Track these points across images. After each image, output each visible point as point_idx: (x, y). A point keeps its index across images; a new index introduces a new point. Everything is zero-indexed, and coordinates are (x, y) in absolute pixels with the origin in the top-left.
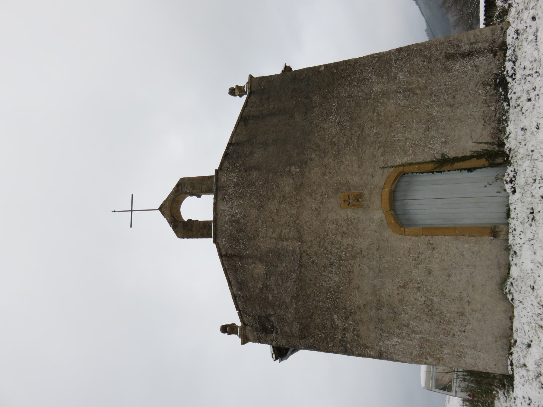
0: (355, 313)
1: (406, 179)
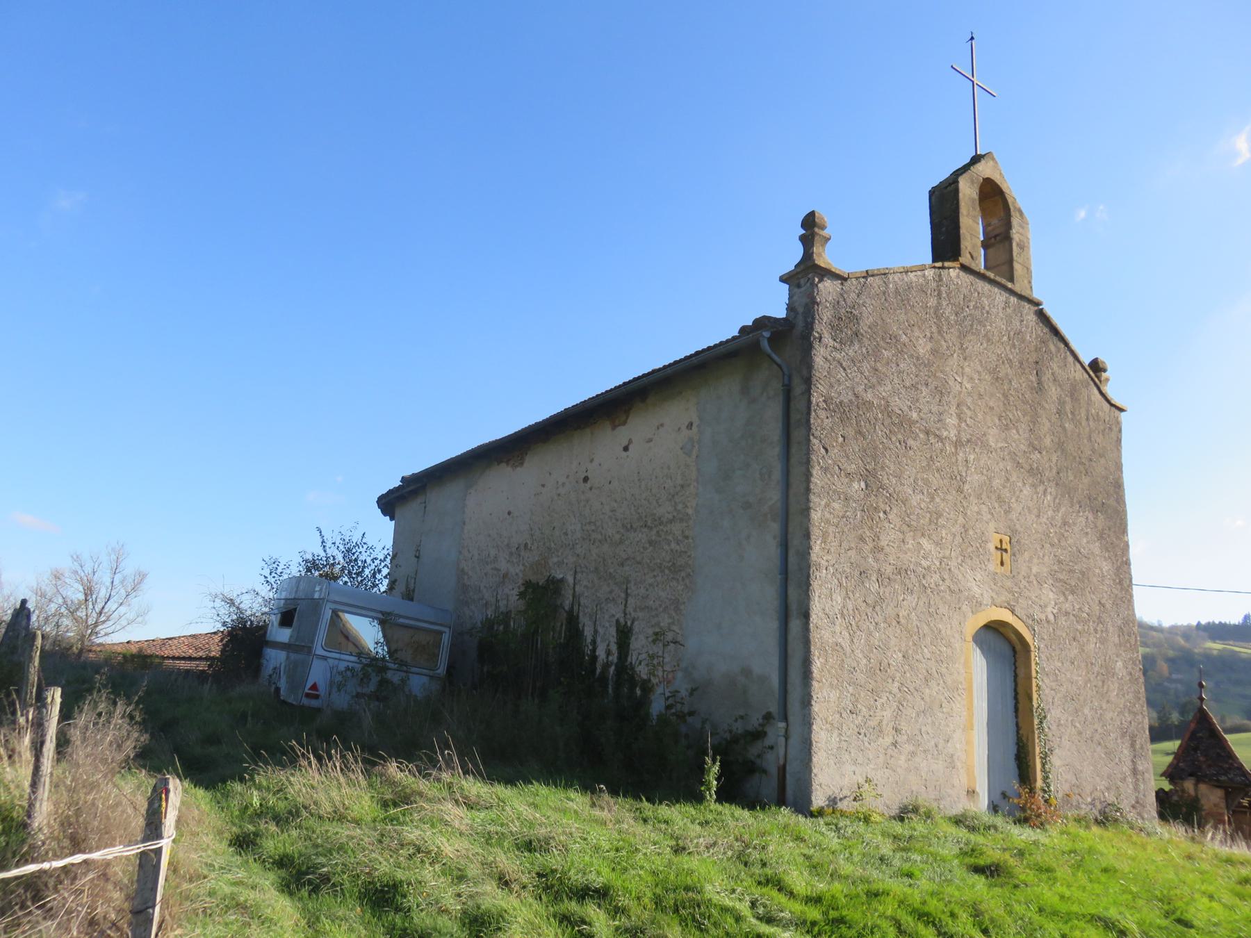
0: (871, 528)
1: (1008, 652)
